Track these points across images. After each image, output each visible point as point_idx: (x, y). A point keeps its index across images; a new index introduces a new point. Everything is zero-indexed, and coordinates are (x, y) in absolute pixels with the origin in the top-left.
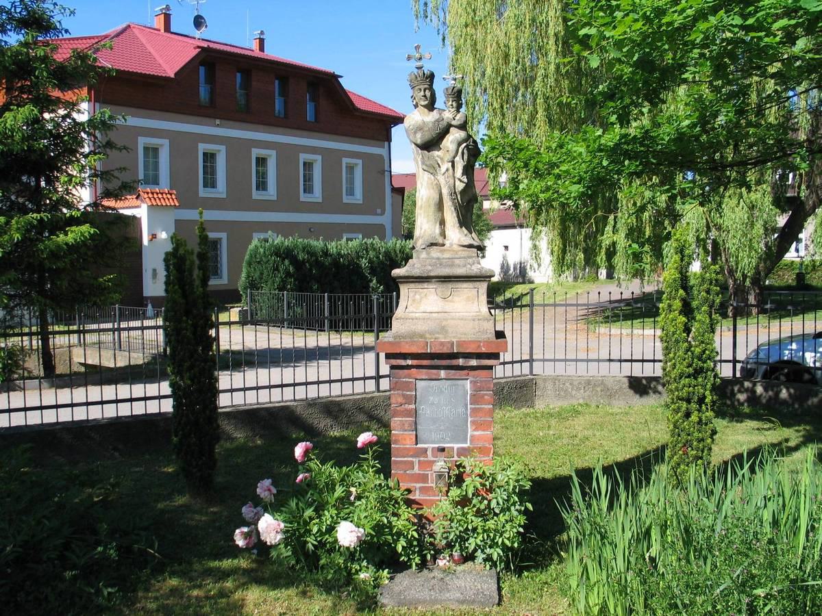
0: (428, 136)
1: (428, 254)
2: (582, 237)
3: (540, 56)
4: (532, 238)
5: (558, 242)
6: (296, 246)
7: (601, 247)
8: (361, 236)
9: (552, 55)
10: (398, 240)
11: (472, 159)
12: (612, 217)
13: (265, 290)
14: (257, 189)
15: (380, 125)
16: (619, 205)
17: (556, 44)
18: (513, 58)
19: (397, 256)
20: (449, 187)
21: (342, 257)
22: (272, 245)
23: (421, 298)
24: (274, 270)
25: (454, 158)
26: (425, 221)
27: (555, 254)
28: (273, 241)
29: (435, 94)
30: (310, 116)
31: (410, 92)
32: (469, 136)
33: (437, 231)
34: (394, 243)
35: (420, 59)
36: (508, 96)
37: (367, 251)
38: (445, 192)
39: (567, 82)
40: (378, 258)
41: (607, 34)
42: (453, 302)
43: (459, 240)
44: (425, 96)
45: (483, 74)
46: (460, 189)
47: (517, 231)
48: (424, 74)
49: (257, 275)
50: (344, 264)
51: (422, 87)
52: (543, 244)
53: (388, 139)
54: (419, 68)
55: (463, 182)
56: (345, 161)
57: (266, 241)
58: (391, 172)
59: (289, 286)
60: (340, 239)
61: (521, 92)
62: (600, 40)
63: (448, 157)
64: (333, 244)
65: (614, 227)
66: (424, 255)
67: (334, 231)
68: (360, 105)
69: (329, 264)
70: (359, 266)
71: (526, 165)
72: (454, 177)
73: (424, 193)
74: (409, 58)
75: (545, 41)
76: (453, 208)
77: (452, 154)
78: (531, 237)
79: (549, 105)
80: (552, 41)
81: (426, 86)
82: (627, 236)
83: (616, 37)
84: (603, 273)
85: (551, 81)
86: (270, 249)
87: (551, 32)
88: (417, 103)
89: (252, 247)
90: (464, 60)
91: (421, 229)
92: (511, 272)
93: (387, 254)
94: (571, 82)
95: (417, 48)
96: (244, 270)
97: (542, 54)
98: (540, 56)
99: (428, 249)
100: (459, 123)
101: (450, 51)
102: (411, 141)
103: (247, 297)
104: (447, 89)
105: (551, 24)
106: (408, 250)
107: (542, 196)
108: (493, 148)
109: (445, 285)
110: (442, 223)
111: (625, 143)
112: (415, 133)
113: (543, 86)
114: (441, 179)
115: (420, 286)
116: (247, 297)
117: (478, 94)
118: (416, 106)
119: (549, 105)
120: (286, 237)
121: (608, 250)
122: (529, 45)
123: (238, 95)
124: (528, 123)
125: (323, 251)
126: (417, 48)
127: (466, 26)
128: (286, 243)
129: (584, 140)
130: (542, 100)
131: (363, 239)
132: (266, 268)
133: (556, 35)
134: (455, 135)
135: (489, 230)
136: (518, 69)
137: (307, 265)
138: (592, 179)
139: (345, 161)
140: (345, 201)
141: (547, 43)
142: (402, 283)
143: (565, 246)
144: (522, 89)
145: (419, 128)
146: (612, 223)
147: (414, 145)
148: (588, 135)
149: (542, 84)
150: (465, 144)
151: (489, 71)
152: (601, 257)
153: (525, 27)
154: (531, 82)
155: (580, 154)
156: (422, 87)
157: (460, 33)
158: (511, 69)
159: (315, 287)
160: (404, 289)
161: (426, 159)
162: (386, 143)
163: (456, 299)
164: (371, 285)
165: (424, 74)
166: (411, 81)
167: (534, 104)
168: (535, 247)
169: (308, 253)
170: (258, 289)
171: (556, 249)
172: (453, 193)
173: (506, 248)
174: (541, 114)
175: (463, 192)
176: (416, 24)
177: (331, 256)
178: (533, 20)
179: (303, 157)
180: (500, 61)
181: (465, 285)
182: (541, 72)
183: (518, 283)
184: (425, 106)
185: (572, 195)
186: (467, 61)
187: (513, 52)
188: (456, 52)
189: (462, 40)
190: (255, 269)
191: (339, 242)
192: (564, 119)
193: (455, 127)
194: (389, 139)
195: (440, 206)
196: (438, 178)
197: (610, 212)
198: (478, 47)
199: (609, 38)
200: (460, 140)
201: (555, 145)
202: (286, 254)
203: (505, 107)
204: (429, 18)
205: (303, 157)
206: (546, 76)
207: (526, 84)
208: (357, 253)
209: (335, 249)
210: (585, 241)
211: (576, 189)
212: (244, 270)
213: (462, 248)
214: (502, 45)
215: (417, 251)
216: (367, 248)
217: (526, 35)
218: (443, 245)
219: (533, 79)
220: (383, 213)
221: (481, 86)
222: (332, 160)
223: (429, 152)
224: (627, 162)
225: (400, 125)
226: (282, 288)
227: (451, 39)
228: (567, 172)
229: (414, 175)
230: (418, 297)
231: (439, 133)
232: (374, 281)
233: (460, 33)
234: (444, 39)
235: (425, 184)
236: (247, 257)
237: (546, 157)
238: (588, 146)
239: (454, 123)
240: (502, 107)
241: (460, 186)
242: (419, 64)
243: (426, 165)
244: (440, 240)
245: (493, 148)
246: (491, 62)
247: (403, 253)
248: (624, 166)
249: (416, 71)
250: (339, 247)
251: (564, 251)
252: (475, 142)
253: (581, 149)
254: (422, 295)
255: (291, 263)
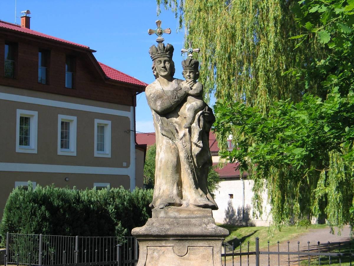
0: (167, 104)
1: (166, 213)
2: (298, 189)
3: (261, 36)
4: (255, 190)
5: (278, 193)
6: (52, 194)
7: (314, 198)
8: (108, 186)
9: (271, 36)
10: (140, 189)
11: (207, 125)
12: (323, 172)
13: (23, 232)
14: (21, 143)
15: (127, 92)
16: (331, 162)
17: (275, 26)
18: (239, 38)
19: (139, 203)
20: (186, 151)
21: (92, 203)
22: (31, 193)
23: (159, 257)
24: (32, 215)
25: (191, 124)
26: (164, 182)
27: (276, 203)
28: (32, 189)
29: (174, 66)
30: (68, 84)
31: (151, 64)
32: (205, 105)
33: (175, 192)
34: (136, 192)
35: (161, 33)
36: (234, 69)
37: (114, 199)
38: (182, 155)
39: (284, 58)
40: (123, 204)
41: (337, 11)
42: (188, 259)
43: (195, 200)
44: (165, 67)
45: (214, 51)
46: (196, 153)
47: (240, 182)
48: (164, 47)
49: (16, 219)
50: (94, 210)
51: (163, 59)
52: (265, 195)
53: (134, 104)
54: (160, 42)
55: (199, 146)
56: (97, 121)
57: (26, 188)
58: (135, 131)
59: (44, 229)
60: (91, 187)
61: (245, 66)
62: (329, 18)
63: (186, 123)
64: (85, 192)
65: (326, 180)
66: (162, 214)
67: (86, 181)
68: (109, 75)
69: (81, 210)
70: (107, 211)
71: (253, 130)
72: (191, 142)
73: (163, 155)
74: (151, 33)
75: (266, 23)
76: (189, 171)
77: (189, 121)
78: (254, 188)
79: (268, 77)
80: (271, 24)
81: (166, 58)
82: (338, 188)
83: (346, 13)
84: (314, 220)
85: (271, 57)
86: (29, 196)
87: (271, 16)
88: (157, 74)
89: (12, 194)
90: (197, 40)
91: (160, 189)
92: (235, 217)
93: (131, 201)
94: (287, 58)
95: (159, 23)
96: (5, 215)
97: (263, 34)
98: (261, 36)
99: (166, 208)
100: (195, 92)
101: (186, 31)
102: (152, 109)
103: (5, 239)
104: (185, 61)
105: (271, 10)
106: (148, 198)
107: (268, 157)
108: (224, 115)
109: (181, 243)
110: (180, 184)
111: (344, 111)
112: (155, 101)
113: (264, 62)
114: (179, 144)
115: (158, 244)
116: (5, 239)
117: (209, 68)
118: (157, 76)
119: (268, 77)
120: (43, 186)
121: (320, 201)
122: (252, 27)
123: (5, 63)
124: (251, 92)
125: (75, 198)
126: (159, 23)
127: (200, 10)
128: (44, 192)
129: (307, 109)
130: (263, 73)
131: (111, 188)
132: (25, 213)
133: (275, 18)
134: (192, 103)
135: (217, 182)
136: (242, 47)
137: (61, 210)
138: (314, 143)
139: (97, 121)
140: (96, 155)
141: (268, 25)
142: (140, 240)
143: (283, 197)
144: (246, 64)
145: (159, 97)
146: (324, 177)
147: (154, 112)
148: (309, 104)
149: (263, 59)
150: (201, 112)
151: (218, 49)
152: (315, 207)
153: (249, 12)
154: (253, 58)
155: (303, 121)
156: (163, 59)
157: (194, 17)
158: (237, 48)
159: (68, 230)
160: (143, 248)
161: (165, 125)
162: (132, 108)
163: (192, 257)
164: (117, 228)
165: (164, 47)
166: (152, 54)
167: (257, 77)
168: (257, 197)
169: (63, 200)
170: (16, 232)
171: (276, 199)
172: (189, 157)
173: (231, 196)
174: (262, 84)
175: (199, 156)
176: (158, 9)
177: (82, 202)
178: (256, 6)
179: (61, 118)
180: (228, 40)
181: (201, 243)
182: (262, 50)
183: (242, 226)
184: (164, 77)
185: (296, 157)
186: (201, 40)
187: (238, 33)
188: (191, 33)
189: (196, 23)
190: (14, 214)
191: (90, 191)
192: (285, 89)
193: (193, 96)
194: (134, 104)
195: (177, 168)
196: (176, 142)
197: (321, 167)
198: (209, 29)
199: (338, 15)
200: (196, 108)
201: (279, 112)
202: (43, 201)
203: (232, 79)
204: (168, 4)
205: (61, 118)
206: (267, 53)
207: (249, 60)
208: (105, 200)
209: (86, 197)
210: (300, 192)
211: (299, 152)
212: (5, 215)
213: (198, 208)
214: (229, 27)
215: (156, 210)
216: (114, 196)
217: (250, 19)
218: (180, 205)
219: (255, 56)
220: (128, 166)
221: (211, 61)
222: (86, 120)
223: (168, 118)
224: (347, 129)
225: (143, 93)
226: (37, 232)
227: (187, 21)
228: (291, 136)
229: (153, 134)
230: (156, 254)
231: (177, 102)
232: (120, 225)
233: (194, 17)
234: (181, 22)
235: (164, 148)
236: (8, 203)
237: (271, 123)
238: (311, 114)
239: (191, 92)
240: (229, 79)
241: (196, 150)
242: (160, 38)
243: (165, 131)
244: (178, 201)
245: (224, 115)
246: (220, 41)
247: (144, 200)
248: (344, 132)
249: (157, 44)
250: (90, 195)
251: (283, 201)
252: (210, 109)
253: (303, 116)
254: (161, 253)
255: (47, 209)
